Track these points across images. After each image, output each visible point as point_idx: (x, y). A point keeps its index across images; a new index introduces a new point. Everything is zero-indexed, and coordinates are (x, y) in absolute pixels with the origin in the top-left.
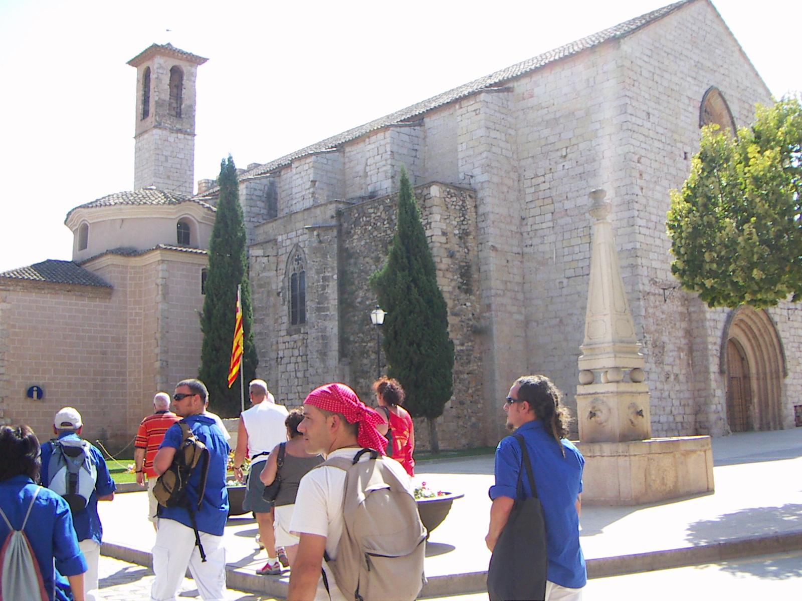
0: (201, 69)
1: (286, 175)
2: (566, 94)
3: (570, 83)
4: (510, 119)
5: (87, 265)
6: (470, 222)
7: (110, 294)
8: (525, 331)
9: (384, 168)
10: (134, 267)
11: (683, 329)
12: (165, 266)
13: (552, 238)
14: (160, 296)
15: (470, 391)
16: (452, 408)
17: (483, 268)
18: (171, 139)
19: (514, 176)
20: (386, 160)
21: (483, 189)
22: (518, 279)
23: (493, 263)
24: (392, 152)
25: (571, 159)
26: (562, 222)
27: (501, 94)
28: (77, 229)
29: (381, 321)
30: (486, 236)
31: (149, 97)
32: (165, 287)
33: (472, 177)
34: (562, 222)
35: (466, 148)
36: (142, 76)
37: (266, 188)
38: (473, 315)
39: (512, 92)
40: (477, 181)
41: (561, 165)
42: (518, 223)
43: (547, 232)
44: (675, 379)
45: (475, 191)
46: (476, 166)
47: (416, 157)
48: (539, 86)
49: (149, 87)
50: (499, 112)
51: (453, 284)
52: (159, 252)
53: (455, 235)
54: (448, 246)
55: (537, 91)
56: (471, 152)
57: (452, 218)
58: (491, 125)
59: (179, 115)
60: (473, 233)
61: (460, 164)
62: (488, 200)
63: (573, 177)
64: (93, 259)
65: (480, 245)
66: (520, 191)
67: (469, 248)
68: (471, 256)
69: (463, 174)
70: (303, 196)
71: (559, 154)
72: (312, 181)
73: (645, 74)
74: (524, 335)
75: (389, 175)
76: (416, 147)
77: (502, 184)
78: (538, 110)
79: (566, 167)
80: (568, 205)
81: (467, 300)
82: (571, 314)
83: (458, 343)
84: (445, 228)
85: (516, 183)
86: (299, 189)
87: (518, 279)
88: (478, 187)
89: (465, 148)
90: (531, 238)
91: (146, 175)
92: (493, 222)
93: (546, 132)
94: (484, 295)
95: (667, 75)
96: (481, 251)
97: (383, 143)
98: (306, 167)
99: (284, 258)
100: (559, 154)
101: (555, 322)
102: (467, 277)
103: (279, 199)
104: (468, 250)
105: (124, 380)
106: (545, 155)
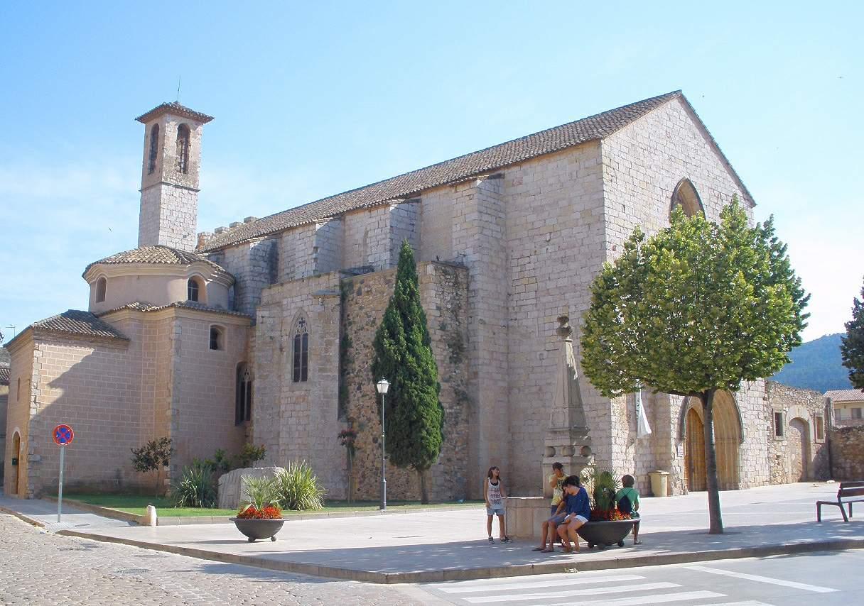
0: (201, 128)
1: (288, 237)
2: (551, 185)
3: (555, 174)
4: (501, 203)
5: (105, 317)
6: (462, 297)
7: (127, 346)
8: (508, 396)
9: (384, 242)
10: (149, 322)
11: (649, 399)
12: (178, 322)
13: (535, 314)
14: (173, 350)
15: (457, 449)
16: (440, 464)
17: (471, 339)
18: (176, 194)
19: (502, 255)
20: (386, 234)
21: (474, 267)
22: (503, 349)
23: (482, 336)
24: (391, 227)
25: (554, 244)
26: (543, 300)
27: (493, 181)
28: (95, 282)
29: (385, 390)
30: (475, 310)
31: (156, 153)
32: (178, 340)
33: (465, 256)
34: (543, 300)
35: (457, 225)
36: (150, 132)
37: (268, 250)
38: (462, 381)
39: (504, 178)
40: (469, 260)
41: (545, 249)
42: (504, 298)
43: (530, 308)
44: (639, 444)
45: (467, 269)
46: (469, 246)
47: (413, 231)
48: (527, 174)
49: (157, 144)
50: (490, 197)
51: (445, 353)
52: (173, 309)
53: (448, 309)
54: (441, 319)
55: (526, 179)
56: (464, 233)
57: (446, 294)
58: (483, 209)
59: (185, 170)
60: (464, 307)
61: (454, 243)
62: (478, 278)
63: (555, 261)
64: (111, 312)
65: (470, 319)
66: (507, 269)
67: (460, 321)
68: (462, 330)
69: (456, 252)
70: (306, 261)
71: (543, 238)
72: (314, 248)
73: (622, 169)
74: (507, 400)
75: (388, 247)
76: (414, 222)
77: (492, 263)
78: (526, 197)
79: (550, 251)
80: (551, 285)
81: (457, 368)
82: (550, 384)
83: (448, 406)
84: (439, 302)
85: (504, 263)
86: (302, 254)
87: (503, 349)
88: (470, 265)
89: (459, 229)
90: (516, 313)
91: (151, 228)
92: (483, 298)
93: (532, 218)
94: (472, 364)
95: (642, 170)
96: (471, 323)
97: (383, 217)
98: (309, 234)
99: (290, 320)
100: (543, 238)
101: (534, 389)
102: (459, 348)
103: (280, 260)
104: (459, 322)
105: (138, 425)
106: (532, 238)
